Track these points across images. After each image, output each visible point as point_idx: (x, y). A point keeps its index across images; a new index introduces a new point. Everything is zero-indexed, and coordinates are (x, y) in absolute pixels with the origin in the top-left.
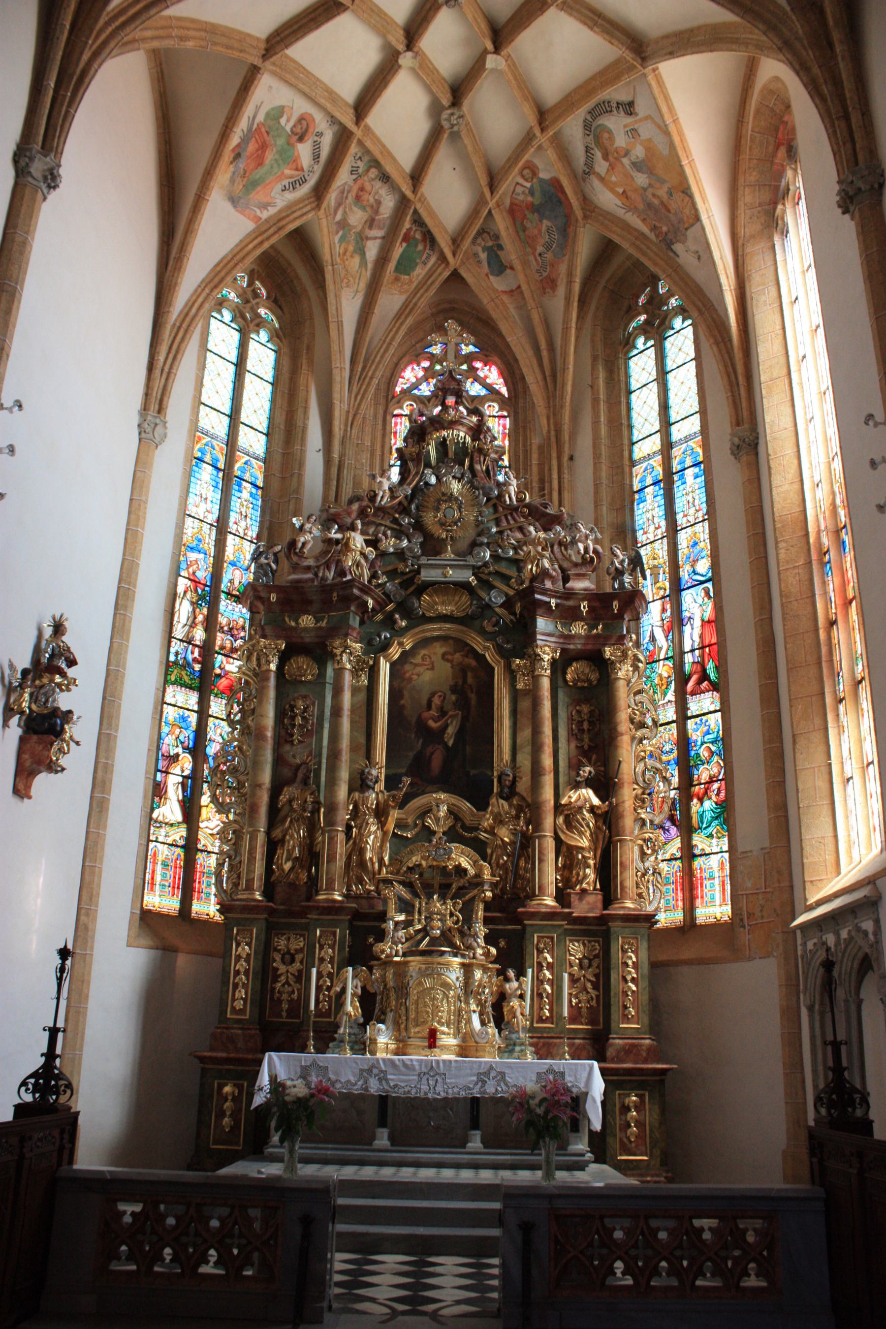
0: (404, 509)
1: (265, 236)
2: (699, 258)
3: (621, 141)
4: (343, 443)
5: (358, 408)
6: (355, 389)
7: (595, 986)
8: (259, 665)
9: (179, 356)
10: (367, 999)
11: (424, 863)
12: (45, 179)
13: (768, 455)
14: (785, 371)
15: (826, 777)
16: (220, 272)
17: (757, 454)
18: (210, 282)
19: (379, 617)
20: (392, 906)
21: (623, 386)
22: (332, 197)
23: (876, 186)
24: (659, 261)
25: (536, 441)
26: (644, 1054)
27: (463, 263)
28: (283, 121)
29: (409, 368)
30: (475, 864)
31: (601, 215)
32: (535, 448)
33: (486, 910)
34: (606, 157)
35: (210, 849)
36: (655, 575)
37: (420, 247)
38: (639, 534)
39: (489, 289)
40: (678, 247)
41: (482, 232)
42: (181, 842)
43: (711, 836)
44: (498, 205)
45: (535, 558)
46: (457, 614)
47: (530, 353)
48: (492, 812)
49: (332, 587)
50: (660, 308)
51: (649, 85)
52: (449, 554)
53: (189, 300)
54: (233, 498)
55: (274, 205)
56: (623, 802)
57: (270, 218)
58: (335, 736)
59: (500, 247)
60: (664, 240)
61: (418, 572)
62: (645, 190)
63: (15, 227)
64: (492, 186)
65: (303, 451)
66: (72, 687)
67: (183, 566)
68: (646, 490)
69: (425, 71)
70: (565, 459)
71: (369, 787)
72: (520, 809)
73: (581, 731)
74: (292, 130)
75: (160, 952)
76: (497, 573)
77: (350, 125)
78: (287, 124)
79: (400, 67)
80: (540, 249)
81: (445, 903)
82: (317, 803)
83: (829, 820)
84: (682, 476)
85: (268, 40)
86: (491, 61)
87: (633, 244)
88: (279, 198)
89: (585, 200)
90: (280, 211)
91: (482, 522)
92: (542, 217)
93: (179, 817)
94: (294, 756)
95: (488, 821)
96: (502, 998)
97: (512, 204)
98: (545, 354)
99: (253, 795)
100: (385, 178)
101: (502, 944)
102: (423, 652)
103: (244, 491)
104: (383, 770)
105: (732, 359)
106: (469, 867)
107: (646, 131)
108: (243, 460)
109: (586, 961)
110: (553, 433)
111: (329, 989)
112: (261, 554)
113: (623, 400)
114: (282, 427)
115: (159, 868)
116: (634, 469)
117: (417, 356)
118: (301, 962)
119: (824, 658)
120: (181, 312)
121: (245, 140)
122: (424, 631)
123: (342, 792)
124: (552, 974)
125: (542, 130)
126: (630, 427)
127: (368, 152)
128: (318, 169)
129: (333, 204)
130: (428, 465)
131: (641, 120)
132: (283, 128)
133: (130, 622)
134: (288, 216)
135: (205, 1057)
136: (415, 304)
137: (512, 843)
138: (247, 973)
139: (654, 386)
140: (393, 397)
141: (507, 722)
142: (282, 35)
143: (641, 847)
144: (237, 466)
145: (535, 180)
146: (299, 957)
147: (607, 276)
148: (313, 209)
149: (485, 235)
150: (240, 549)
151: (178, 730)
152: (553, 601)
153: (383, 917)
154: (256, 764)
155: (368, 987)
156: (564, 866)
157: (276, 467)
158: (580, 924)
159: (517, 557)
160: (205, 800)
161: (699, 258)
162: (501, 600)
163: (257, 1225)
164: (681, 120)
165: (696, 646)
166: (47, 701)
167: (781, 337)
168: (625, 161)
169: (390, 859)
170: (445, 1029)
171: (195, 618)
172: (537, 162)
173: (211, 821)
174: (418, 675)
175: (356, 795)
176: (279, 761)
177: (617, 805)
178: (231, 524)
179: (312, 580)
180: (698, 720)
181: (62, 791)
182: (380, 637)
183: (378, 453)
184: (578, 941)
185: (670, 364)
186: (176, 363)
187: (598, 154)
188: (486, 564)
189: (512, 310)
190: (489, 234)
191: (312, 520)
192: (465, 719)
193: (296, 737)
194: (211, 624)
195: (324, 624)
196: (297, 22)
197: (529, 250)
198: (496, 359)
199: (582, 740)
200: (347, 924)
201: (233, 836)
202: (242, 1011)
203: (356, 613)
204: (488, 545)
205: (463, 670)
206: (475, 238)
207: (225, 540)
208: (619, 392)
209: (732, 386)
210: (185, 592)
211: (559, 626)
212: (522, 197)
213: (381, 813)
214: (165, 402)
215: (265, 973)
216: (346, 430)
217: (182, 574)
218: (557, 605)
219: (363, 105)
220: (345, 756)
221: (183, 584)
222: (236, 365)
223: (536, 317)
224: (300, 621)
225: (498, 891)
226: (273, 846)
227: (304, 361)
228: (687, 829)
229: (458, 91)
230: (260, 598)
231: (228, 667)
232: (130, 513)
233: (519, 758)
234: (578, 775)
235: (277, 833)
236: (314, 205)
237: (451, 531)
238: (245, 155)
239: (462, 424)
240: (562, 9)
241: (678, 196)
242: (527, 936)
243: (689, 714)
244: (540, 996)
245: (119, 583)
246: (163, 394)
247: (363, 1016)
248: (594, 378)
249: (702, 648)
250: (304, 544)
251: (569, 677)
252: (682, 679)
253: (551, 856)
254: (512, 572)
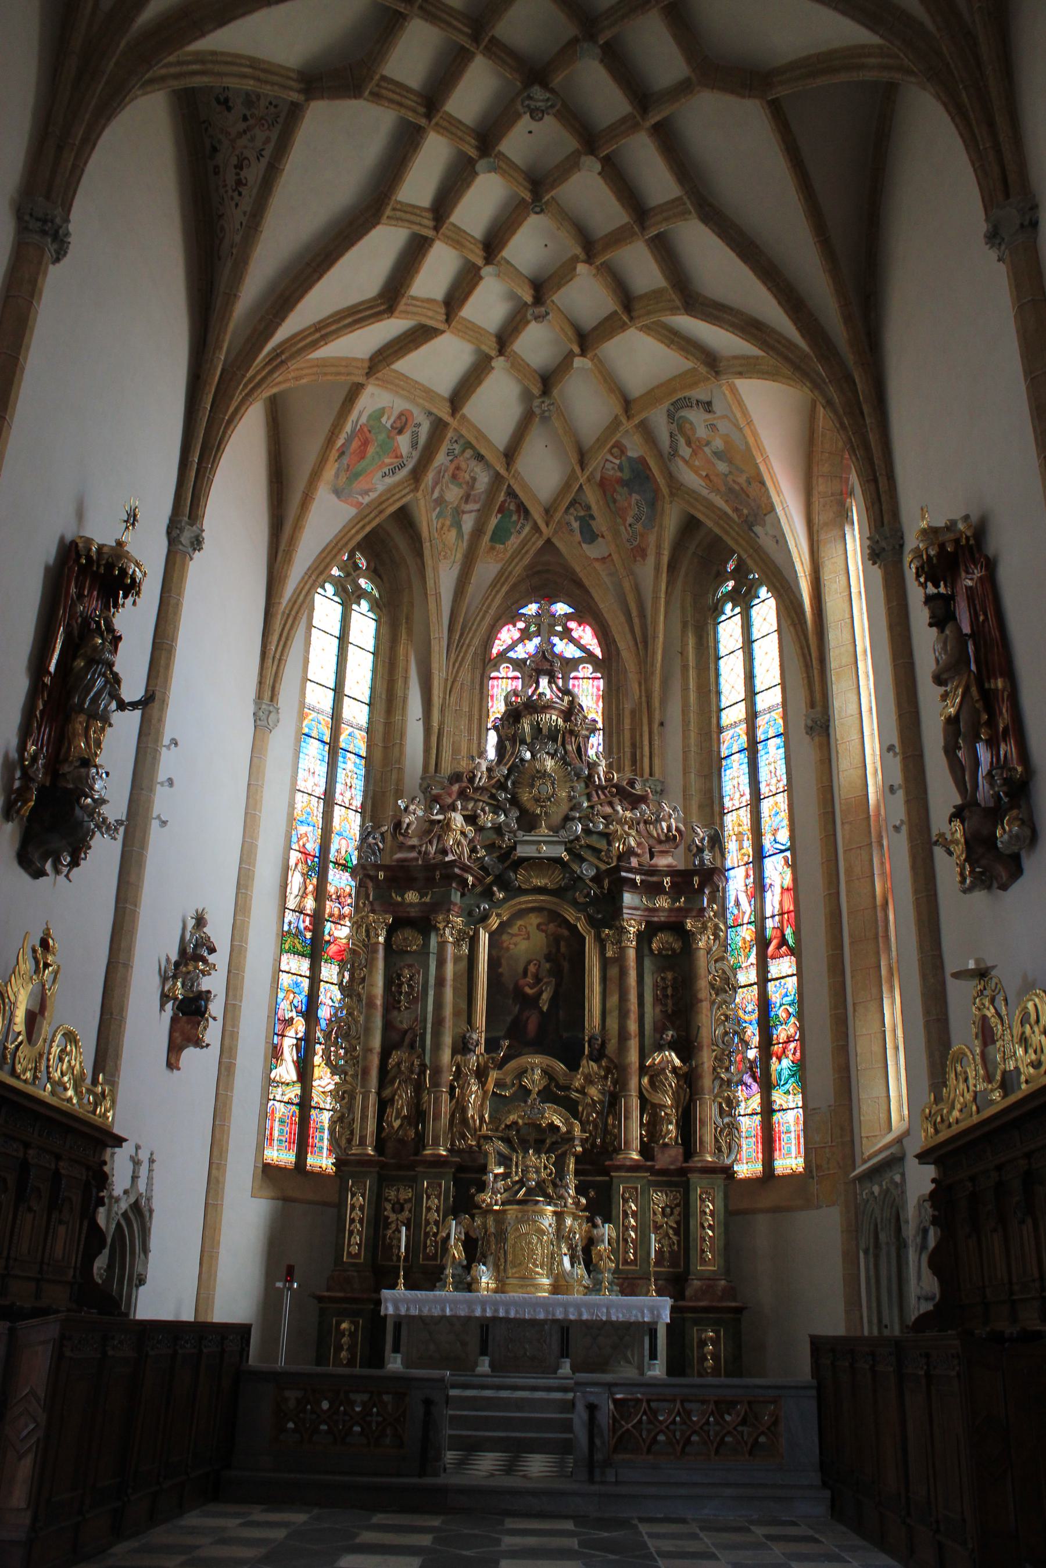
0: (501, 786)
1: (367, 520)
2: (777, 542)
3: (702, 432)
4: (442, 711)
5: (456, 676)
6: (453, 656)
7: (677, 1232)
8: (368, 935)
10: (470, 1244)
11: (520, 1122)
12: (192, 544)
13: (836, 740)
14: (853, 660)
15: (880, 1042)
16: (325, 558)
17: (828, 735)
18: (316, 569)
19: (479, 889)
20: (492, 1160)
21: (712, 651)
22: (430, 476)
23: (897, 547)
25: (628, 706)
26: (720, 1294)
27: (555, 532)
28: (384, 420)
29: (505, 629)
30: (567, 1123)
32: (627, 713)
33: (576, 1163)
34: (689, 443)
35: (322, 1106)
36: (740, 841)
37: (515, 518)
38: (726, 800)
39: (584, 556)
40: (758, 529)
41: (573, 503)
42: (296, 1101)
43: (788, 1092)
44: (589, 480)
45: (622, 836)
48: (583, 1073)
49: (435, 867)
51: (724, 394)
54: (339, 770)
55: (375, 490)
56: (702, 1064)
57: (371, 502)
58: (439, 1005)
59: (592, 517)
60: (746, 521)
61: (514, 848)
62: (726, 476)
63: (170, 591)
64: (582, 464)
65: (404, 721)
66: (212, 972)
67: (294, 839)
68: (732, 757)
69: (518, 366)
70: (656, 725)
71: (470, 1050)
72: (608, 1071)
73: (666, 996)
74: (392, 426)
75: (280, 1203)
76: (589, 847)
78: (387, 421)
79: (493, 368)
80: (630, 520)
81: (539, 1157)
82: (423, 1066)
83: (882, 1081)
84: (766, 746)
86: (578, 362)
88: (379, 484)
91: (574, 797)
93: (293, 1076)
94: (401, 1022)
95: (578, 1081)
96: (590, 1243)
98: (636, 621)
99: (365, 1058)
100: (480, 457)
101: (592, 1194)
102: (519, 923)
103: (349, 762)
104: (483, 1035)
105: (807, 640)
106: (560, 1125)
107: (723, 427)
108: (347, 732)
109: (668, 1210)
110: (644, 699)
111: (435, 1235)
112: (369, 834)
113: (712, 666)
114: (384, 696)
115: (277, 1124)
117: (513, 617)
118: (410, 1211)
119: (881, 934)
120: (290, 600)
121: (349, 440)
122: (520, 903)
123: (446, 1056)
124: (636, 1221)
125: (628, 418)
126: (718, 693)
128: (416, 455)
130: (523, 742)
132: (385, 426)
134: (388, 499)
135: (324, 1297)
136: (510, 573)
137: (601, 1102)
138: (361, 1221)
139: (740, 654)
141: (597, 988)
142: (385, 355)
143: (720, 1104)
144: (342, 737)
146: (407, 1206)
148: (412, 491)
150: (349, 825)
151: (292, 996)
152: (638, 877)
153: (484, 1169)
154: (368, 1030)
155: (471, 1234)
156: (648, 1122)
158: (664, 1176)
159: (607, 831)
160: (317, 1060)
161: (777, 542)
162: (592, 873)
163: (390, 1407)
164: (755, 422)
165: (776, 913)
166: (192, 985)
167: (849, 626)
168: (706, 449)
169: (490, 1116)
170: (538, 1270)
171: (306, 888)
172: (625, 442)
173: (324, 1080)
174: (515, 945)
175: (459, 1057)
176: (388, 1026)
177: (697, 1066)
178: (337, 796)
179: (417, 859)
180: (777, 982)
181: (200, 1062)
182: (479, 908)
183: (476, 717)
184: (661, 1192)
185: (756, 634)
186: (287, 650)
187: (682, 441)
188: (578, 838)
190: (580, 504)
192: (558, 985)
193: (404, 1004)
194: (321, 894)
195: (427, 899)
197: (619, 520)
198: (591, 620)
199: (666, 1005)
200: (451, 1176)
201: (343, 1095)
202: (357, 1256)
204: (580, 819)
205: (555, 940)
206: (568, 508)
207: (332, 811)
209: (807, 666)
210: (296, 865)
211: (644, 900)
213: (481, 1074)
215: (377, 1223)
216: (444, 698)
217: (294, 847)
218: (642, 881)
220: (449, 1023)
221: (294, 856)
223: (627, 585)
224: (406, 896)
225: (588, 1146)
226: (383, 1104)
227: (404, 631)
228: (767, 1086)
231: (337, 934)
233: (608, 1021)
234: (662, 1038)
235: (387, 1093)
236: (413, 487)
237: (545, 806)
239: (554, 708)
240: (641, 330)
242: (614, 1187)
243: (770, 977)
244: (625, 1241)
245: (240, 863)
247: (466, 1258)
248: (684, 645)
249: (782, 914)
250: (408, 825)
251: (654, 946)
252: (762, 942)
253: (636, 1113)
254: (602, 845)
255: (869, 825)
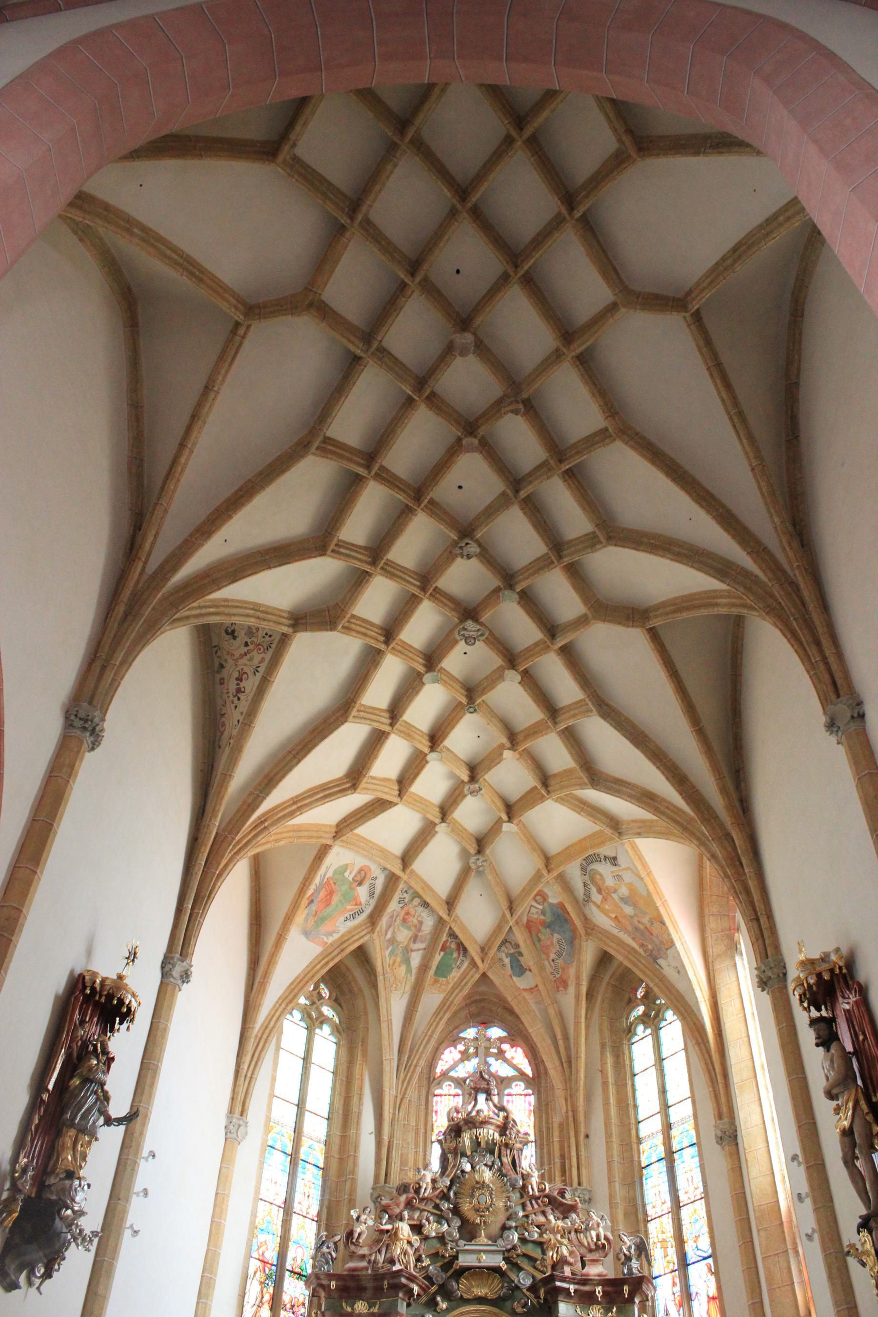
0: (445, 1197)
1: (330, 957)
3: (610, 882)
5: (405, 1093)
6: (402, 1076)
9: (260, 1063)
12: (182, 977)
13: (745, 1149)
14: (751, 1074)
16: (294, 988)
18: (285, 999)
19: (424, 1299)
21: (628, 1069)
22: (384, 921)
23: (781, 975)
24: (648, 972)
25: (557, 1120)
27: (490, 967)
28: (346, 874)
29: (448, 1050)
31: (600, 933)
32: (556, 1126)
34: (599, 891)
37: (455, 955)
39: (514, 987)
41: (505, 942)
44: (517, 923)
46: (490, 1296)
47: (549, 1041)
50: (654, 1003)
51: (627, 851)
52: (483, 1239)
53: (268, 1015)
57: (334, 942)
59: (521, 954)
61: (456, 1257)
62: (632, 917)
64: (511, 909)
65: (358, 1135)
67: (255, 1247)
69: (457, 831)
76: (525, 1255)
77: (398, 872)
78: (349, 876)
85: (337, 825)
86: (506, 827)
87: (626, 957)
88: (341, 927)
89: (586, 920)
90: (343, 936)
91: (510, 1207)
92: (553, 931)
97: (528, 921)
98: (561, 1043)
100: (426, 905)
107: (628, 877)
110: (570, 1114)
112: (323, 1242)
113: (629, 1082)
114: (341, 1112)
116: (641, 1146)
117: (454, 1041)
121: (317, 891)
125: (549, 871)
126: (636, 1107)
127: (411, 887)
128: (373, 902)
129: (384, 926)
130: (463, 1155)
131: (623, 870)
133: (210, 1310)
134: (348, 939)
136: (452, 1002)
139: (653, 1071)
140: (434, 1079)
142: (349, 822)
145: (546, 904)
147: (610, 972)
148: (368, 933)
149: (507, 944)
157: (335, 1148)
159: (541, 1240)
161: (679, 972)
162: (528, 1282)
164: (654, 872)
167: (747, 1044)
168: (614, 895)
171: (263, 1297)
172: (546, 890)
179: (367, 1269)
183: (422, 1130)
186: (257, 1069)
187: (594, 890)
188: (514, 1248)
189: (533, 1006)
190: (511, 943)
191: (367, 1211)
195: (375, 1310)
196: (359, 813)
197: (543, 956)
203: (403, 1300)
206: (500, 947)
208: (624, 1074)
210: (255, 1273)
211: (578, 1310)
212: (535, 915)
214: (247, 1104)
216: (394, 1114)
218: (575, 1291)
219: (407, 858)
221: (254, 1264)
222: (304, 1059)
223: (552, 1011)
224: (356, 1306)
229: (481, 843)
230: (322, 1286)
232: (215, 1206)
238: (316, 901)
239: (491, 1123)
241: (657, 925)
245: (203, 1272)
246: (245, 1097)
248: (603, 1063)
250: (360, 1235)
254: (536, 1253)
255: (783, 1232)
